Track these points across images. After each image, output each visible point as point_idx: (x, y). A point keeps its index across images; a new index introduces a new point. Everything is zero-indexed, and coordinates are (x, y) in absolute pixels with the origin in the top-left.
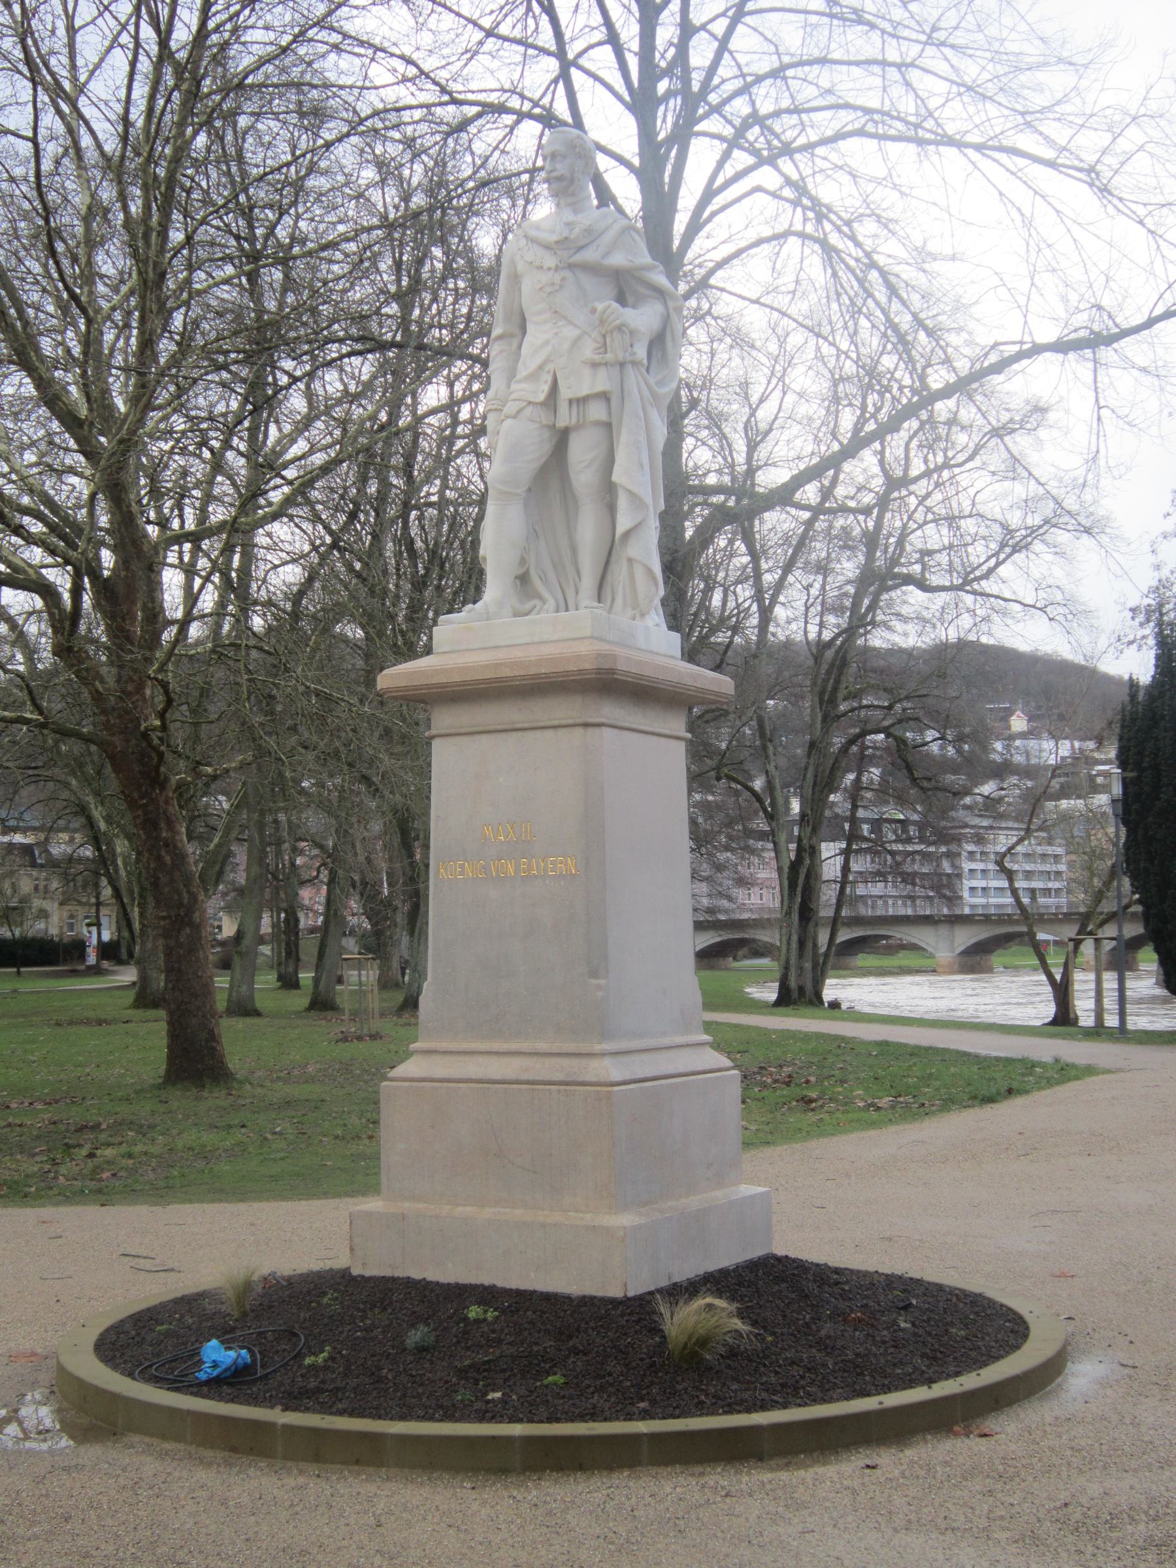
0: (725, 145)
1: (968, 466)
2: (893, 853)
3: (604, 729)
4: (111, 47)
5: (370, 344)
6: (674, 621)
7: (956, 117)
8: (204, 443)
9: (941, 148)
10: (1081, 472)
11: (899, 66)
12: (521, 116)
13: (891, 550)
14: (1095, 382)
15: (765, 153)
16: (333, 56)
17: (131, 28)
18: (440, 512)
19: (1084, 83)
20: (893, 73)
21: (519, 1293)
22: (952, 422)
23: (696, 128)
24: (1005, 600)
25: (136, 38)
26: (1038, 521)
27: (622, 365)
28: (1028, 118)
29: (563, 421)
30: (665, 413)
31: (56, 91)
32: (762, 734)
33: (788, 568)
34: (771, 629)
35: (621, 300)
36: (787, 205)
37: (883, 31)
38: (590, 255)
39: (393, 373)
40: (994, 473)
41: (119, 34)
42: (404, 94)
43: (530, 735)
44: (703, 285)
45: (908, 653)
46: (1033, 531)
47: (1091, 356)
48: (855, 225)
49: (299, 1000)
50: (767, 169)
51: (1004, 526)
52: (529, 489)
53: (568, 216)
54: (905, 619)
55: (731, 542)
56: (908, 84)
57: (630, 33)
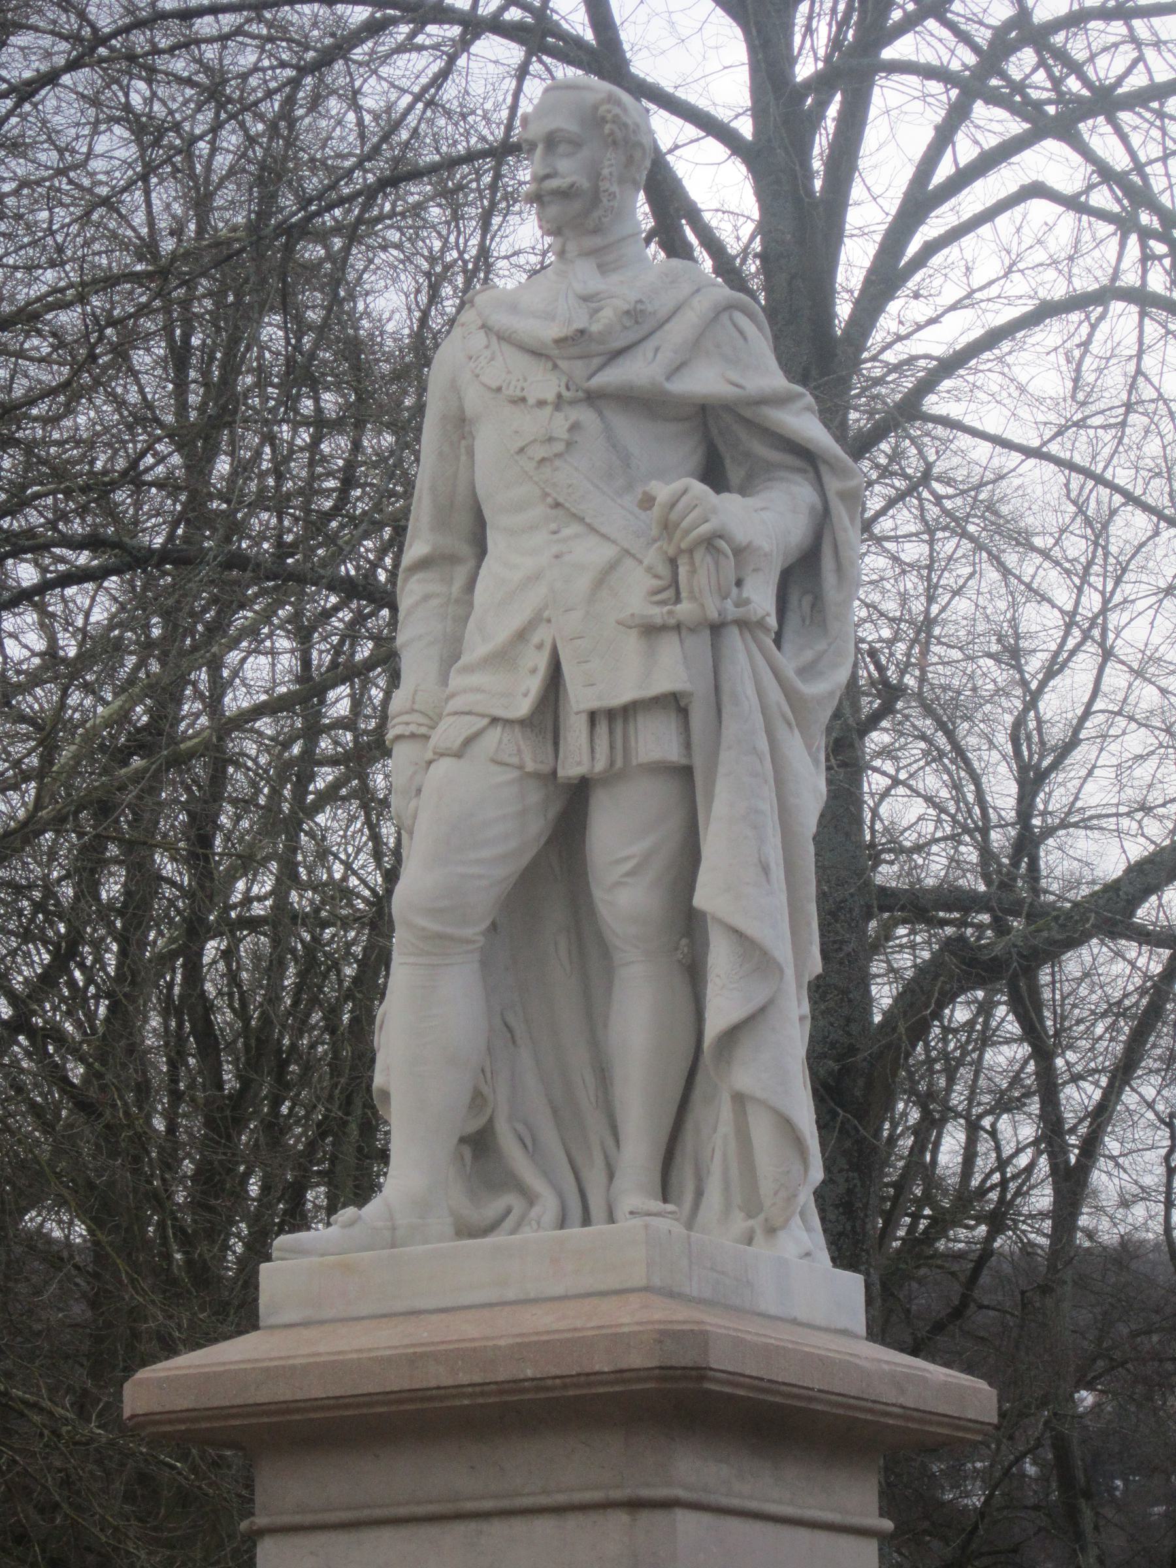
0: (954, 93)
3: (680, 1514)
6: (847, 1249)
18: (276, 942)
23: (887, 54)
27: (716, 629)
29: (577, 760)
30: (821, 742)
32: (1067, 1481)
33: (1123, 1073)
34: (1084, 1221)
35: (714, 474)
36: (1105, 229)
39: (166, 615)
43: (497, 1528)
44: (909, 410)
50: (1051, 145)
52: (494, 926)
53: (586, 276)
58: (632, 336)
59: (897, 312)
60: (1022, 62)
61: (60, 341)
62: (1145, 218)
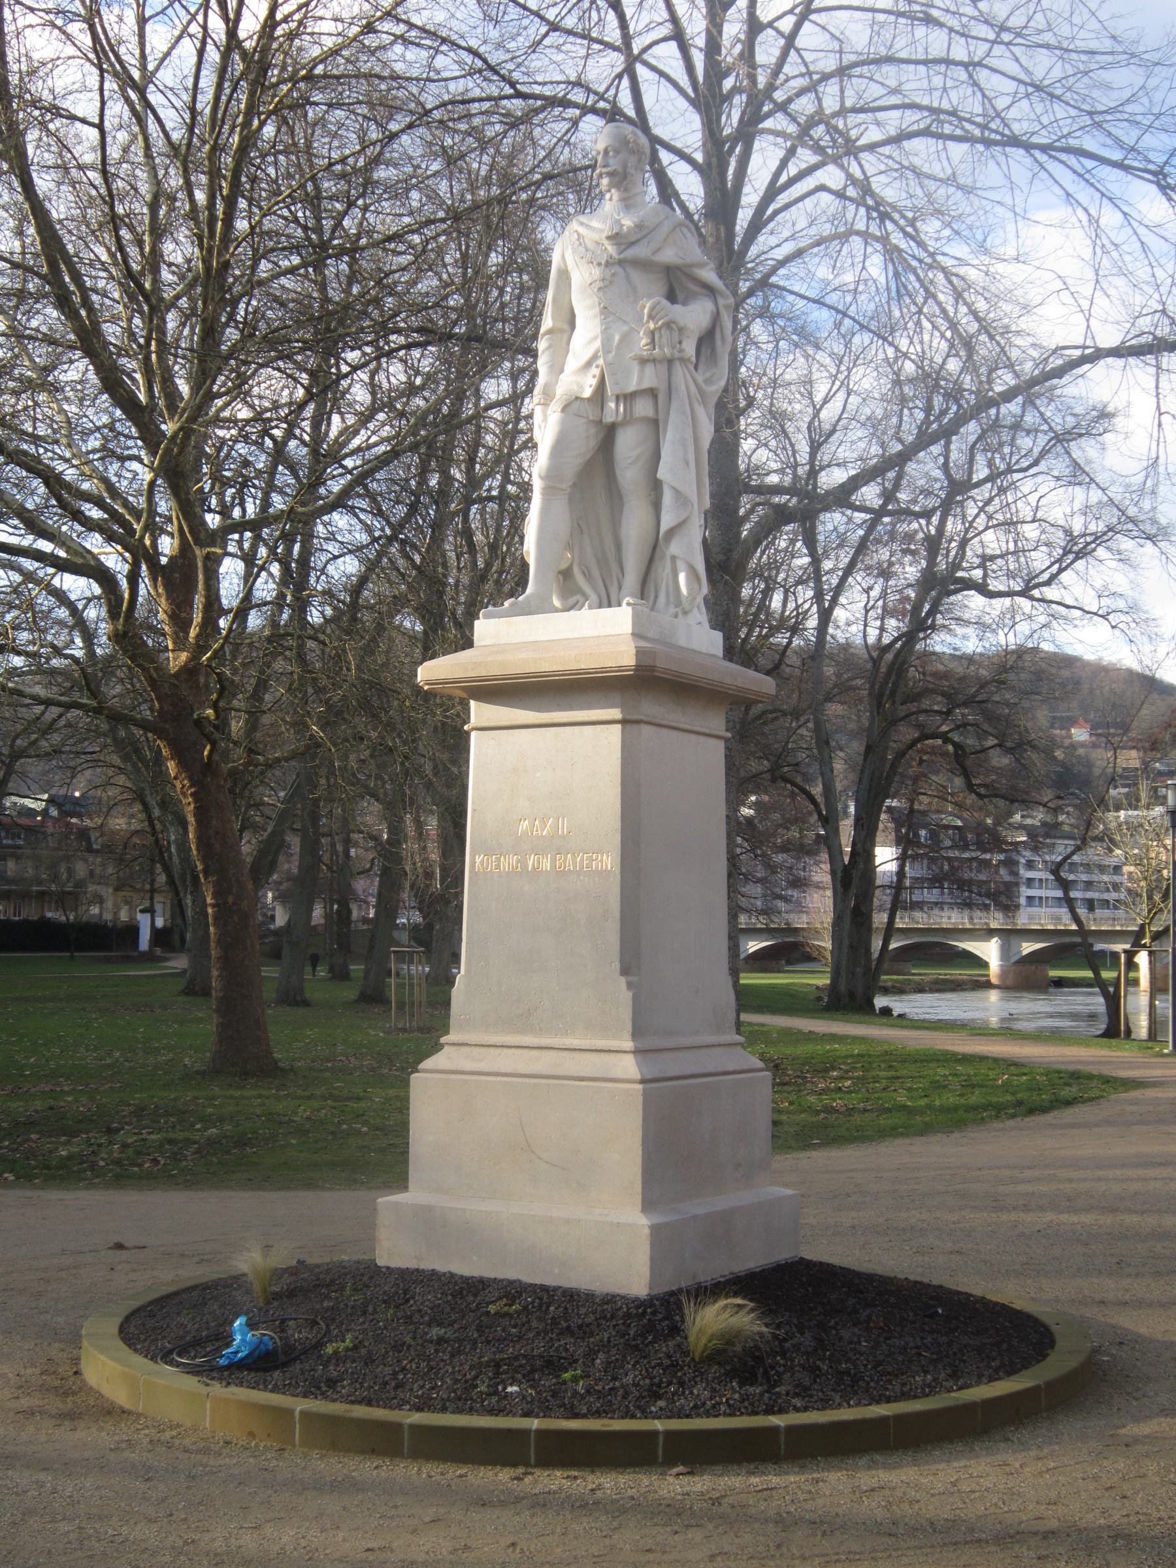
1: (1032, 471)
2: (949, 859)
4: (180, 37)
5: (430, 335)
7: (1023, 117)
8: (265, 432)
9: (1008, 149)
10: (1141, 477)
11: (965, 65)
12: (586, 110)
13: (953, 553)
14: (1157, 387)
15: (829, 151)
16: (398, 48)
17: (200, 18)
18: (500, 505)
19: (1152, 83)
20: (961, 74)
21: (544, 1288)
22: (1016, 426)
24: (1068, 607)
25: (205, 27)
26: (1101, 527)
27: (670, 362)
28: (1097, 119)
30: (712, 411)
31: (125, 80)
33: (849, 571)
34: (831, 631)
35: (672, 297)
37: (951, 30)
38: (641, 251)
40: (1058, 478)
41: (189, 23)
42: (474, 87)
45: (970, 659)
46: (1098, 539)
47: (1154, 362)
48: (918, 224)
49: (350, 993)
50: (831, 168)
51: (1068, 532)
52: (574, 485)
54: (968, 623)
55: (793, 542)
56: (976, 84)
57: (696, 26)
58: (639, 236)
59: (764, 240)
60: (819, 131)
61: (411, 246)
62: (870, 202)
